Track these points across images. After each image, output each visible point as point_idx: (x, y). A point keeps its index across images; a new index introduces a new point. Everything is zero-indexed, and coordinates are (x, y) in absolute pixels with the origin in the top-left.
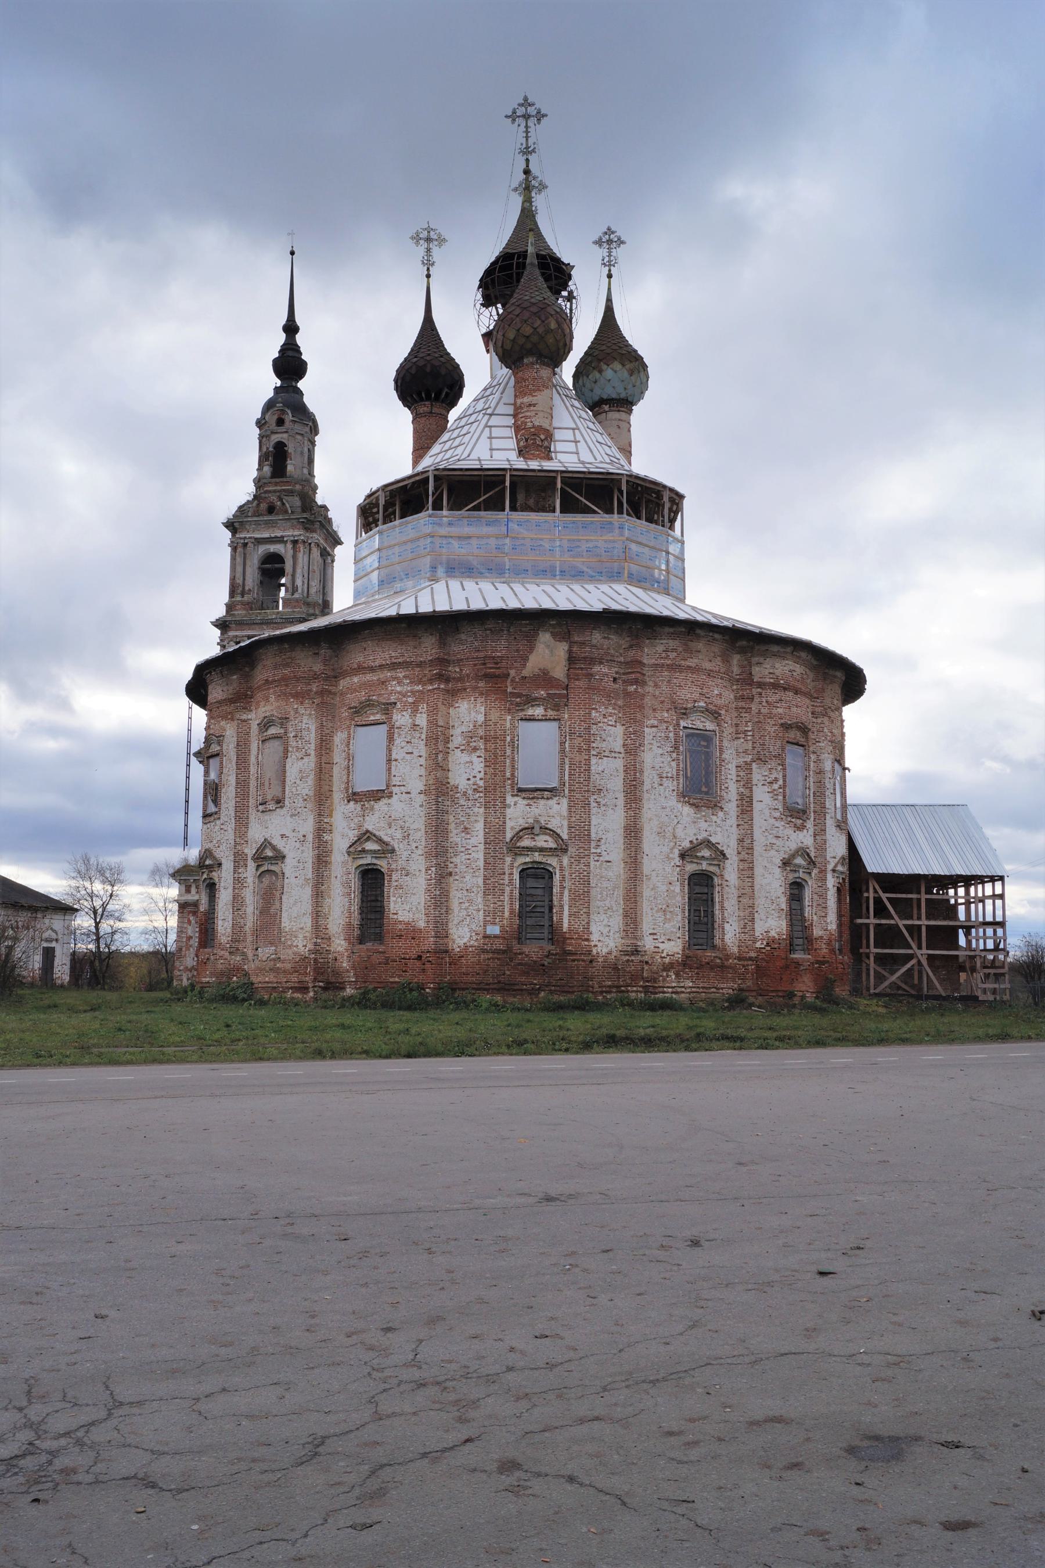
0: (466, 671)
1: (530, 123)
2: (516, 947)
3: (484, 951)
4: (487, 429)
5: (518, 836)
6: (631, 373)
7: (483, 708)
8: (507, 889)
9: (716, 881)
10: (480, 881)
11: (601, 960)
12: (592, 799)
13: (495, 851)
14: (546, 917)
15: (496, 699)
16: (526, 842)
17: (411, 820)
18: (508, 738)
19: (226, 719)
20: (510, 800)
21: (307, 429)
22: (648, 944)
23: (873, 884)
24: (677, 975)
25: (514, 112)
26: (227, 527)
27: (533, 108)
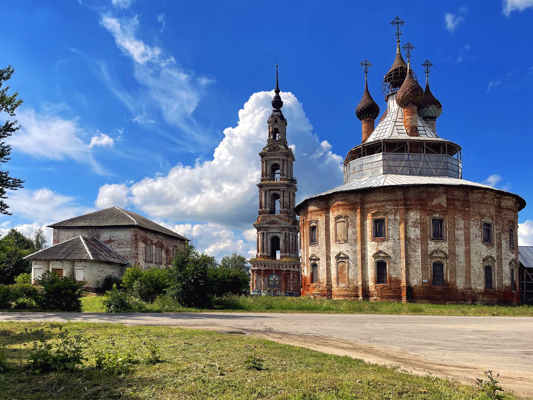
0: (412, 203)
1: (399, 25)
2: (433, 287)
3: (422, 287)
4: (396, 127)
5: (432, 253)
6: (438, 108)
7: (419, 215)
8: (430, 269)
9: (492, 268)
10: (420, 266)
11: (459, 291)
12: (455, 243)
13: (425, 257)
14: (442, 278)
15: (423, 212)
16: (435, 255)
17: (395, 248)
18: (428, 223)
19: (319, 215)
20: (429, 242)
21: (284, 124)
22: (473, 286)
23: (525, 271)
24: (482, 296)
25: (393, 22)
26: (260, 155)
27: (400, 20)
